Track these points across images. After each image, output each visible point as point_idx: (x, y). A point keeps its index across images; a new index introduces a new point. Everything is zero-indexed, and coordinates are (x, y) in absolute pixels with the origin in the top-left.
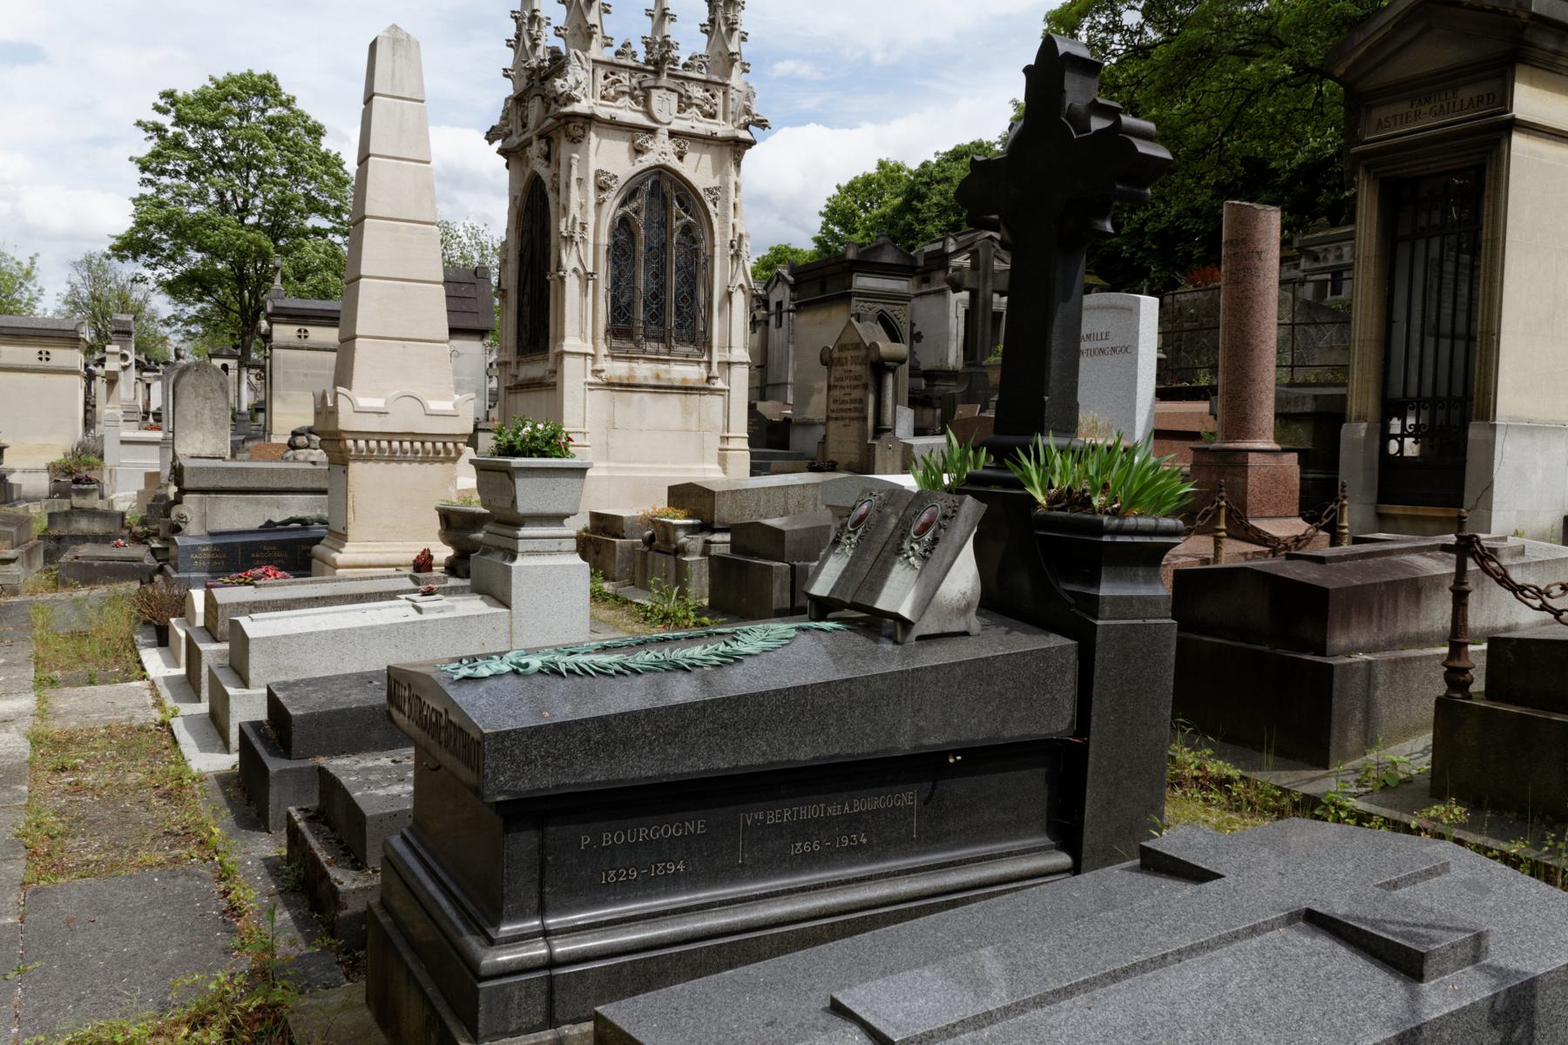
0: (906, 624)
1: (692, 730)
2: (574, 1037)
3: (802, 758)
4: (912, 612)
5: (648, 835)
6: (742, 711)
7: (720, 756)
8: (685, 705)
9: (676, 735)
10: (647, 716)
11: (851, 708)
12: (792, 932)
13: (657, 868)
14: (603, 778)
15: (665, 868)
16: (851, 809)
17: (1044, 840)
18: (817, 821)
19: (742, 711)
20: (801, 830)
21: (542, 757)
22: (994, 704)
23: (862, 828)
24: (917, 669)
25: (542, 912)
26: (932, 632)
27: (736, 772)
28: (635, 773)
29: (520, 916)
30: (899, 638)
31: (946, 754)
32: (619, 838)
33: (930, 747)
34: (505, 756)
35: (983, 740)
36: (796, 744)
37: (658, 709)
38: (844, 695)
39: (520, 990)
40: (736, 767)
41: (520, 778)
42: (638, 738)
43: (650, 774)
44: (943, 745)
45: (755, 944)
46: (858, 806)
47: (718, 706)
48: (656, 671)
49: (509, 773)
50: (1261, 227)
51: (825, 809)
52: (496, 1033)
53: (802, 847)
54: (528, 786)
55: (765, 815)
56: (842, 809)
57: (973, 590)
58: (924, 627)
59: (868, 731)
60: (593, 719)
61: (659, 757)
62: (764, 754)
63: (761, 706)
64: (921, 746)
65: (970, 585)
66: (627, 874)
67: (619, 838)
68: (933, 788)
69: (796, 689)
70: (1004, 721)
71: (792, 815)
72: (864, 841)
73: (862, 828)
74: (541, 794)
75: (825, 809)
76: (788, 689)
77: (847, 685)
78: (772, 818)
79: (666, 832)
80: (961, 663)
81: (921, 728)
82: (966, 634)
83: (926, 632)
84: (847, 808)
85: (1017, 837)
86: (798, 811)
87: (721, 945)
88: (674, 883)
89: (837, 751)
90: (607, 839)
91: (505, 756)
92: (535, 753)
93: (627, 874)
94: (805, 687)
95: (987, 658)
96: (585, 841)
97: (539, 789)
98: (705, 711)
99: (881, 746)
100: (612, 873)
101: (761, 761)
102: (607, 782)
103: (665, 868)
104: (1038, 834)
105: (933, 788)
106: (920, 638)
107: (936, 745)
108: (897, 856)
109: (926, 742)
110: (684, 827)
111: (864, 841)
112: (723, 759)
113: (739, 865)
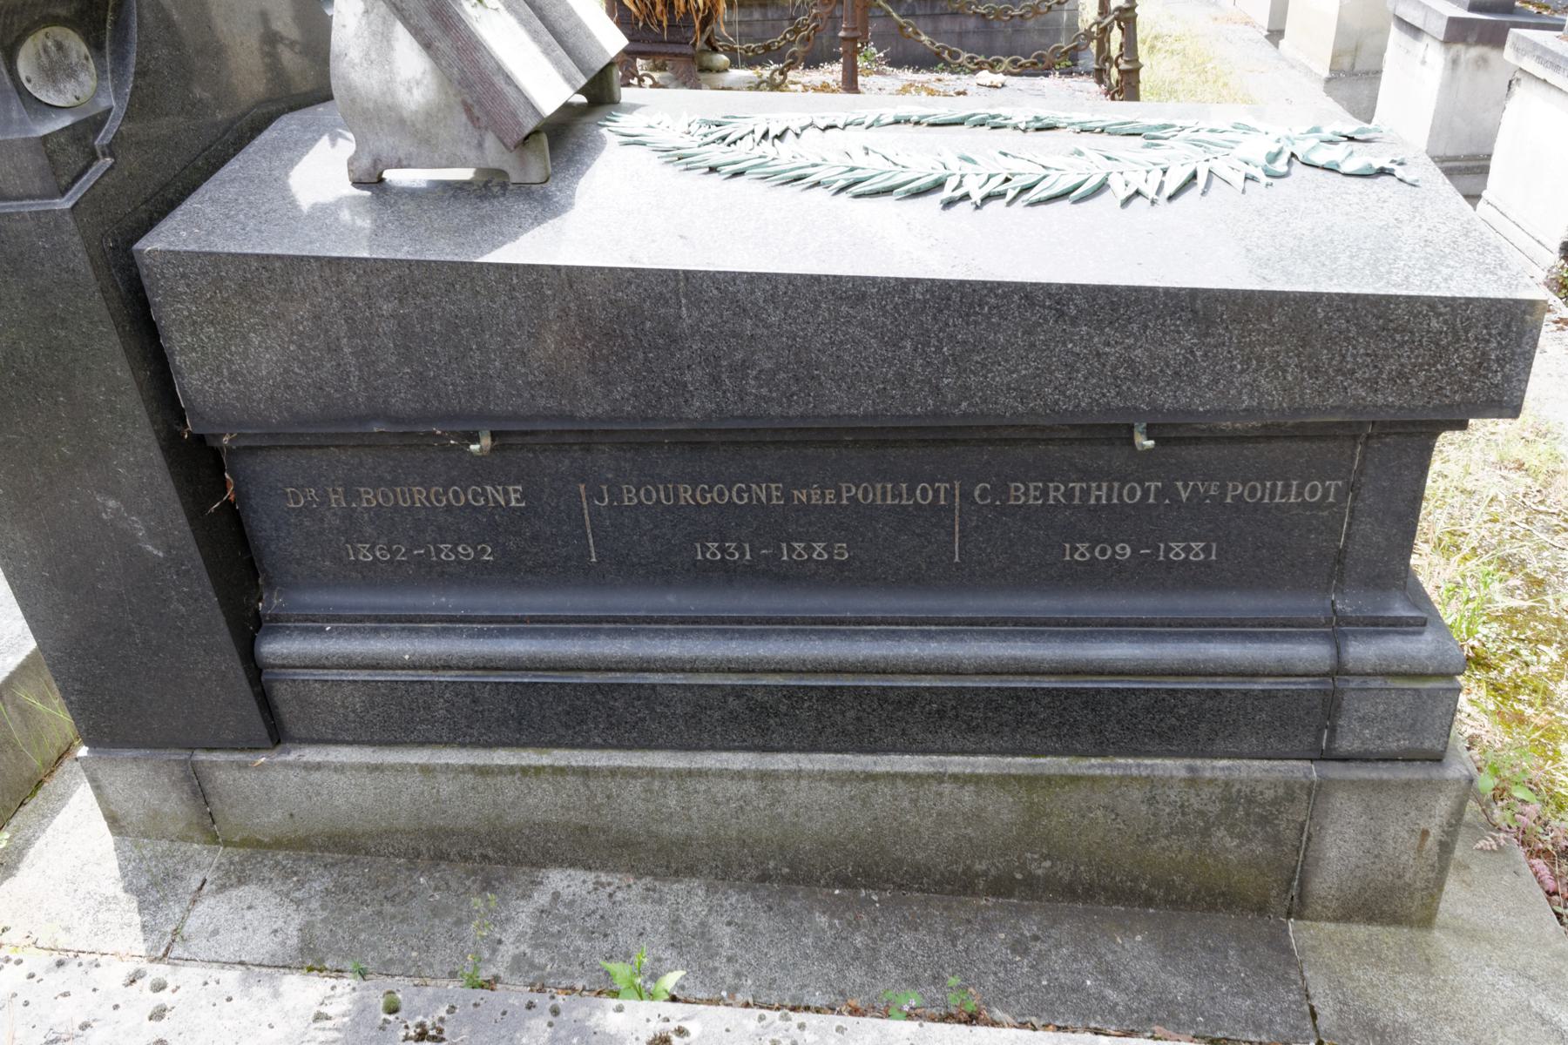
67: (648, 495)
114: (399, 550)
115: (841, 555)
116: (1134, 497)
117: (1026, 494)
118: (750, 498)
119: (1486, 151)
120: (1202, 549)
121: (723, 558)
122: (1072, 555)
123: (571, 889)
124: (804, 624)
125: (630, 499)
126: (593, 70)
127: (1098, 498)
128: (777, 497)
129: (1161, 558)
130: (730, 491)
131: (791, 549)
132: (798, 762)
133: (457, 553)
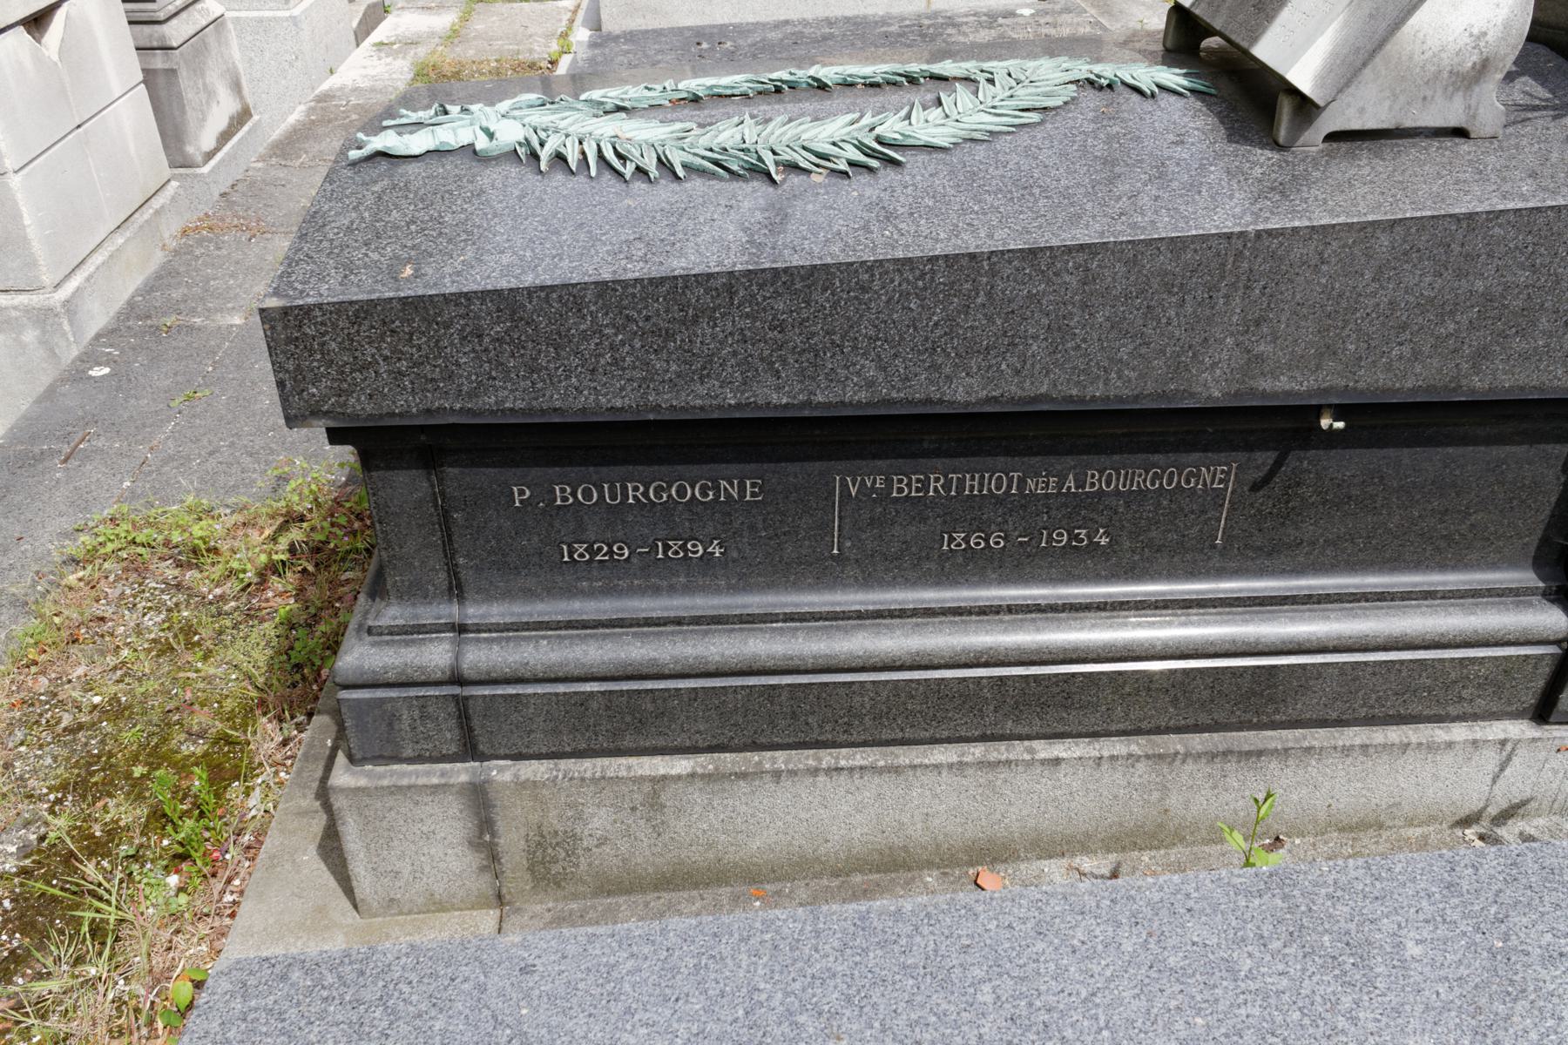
0: (1305, 107)
1: (704, 327)
2: (505, 785)
3: (961, 396)
4: (1321, 80)
5: (646, 494)
6: (820, 298)
7: (771, 381)
8: (686, 278)
9: (669, 336)
10: (600, 296)
11: (1084, 306)
12: (918, 681)
13: (667, 548)
14: (520, 405)
15: (683, 547)
16: (1080, 484)
17: (1526, 577)
18: (1000, 501)
19: (820, 298)
20: (971, 512)
21: (386, 359)
22: (1464, 319)
23: (1103, 519)
24: (1269, 232)
25: (456, 590)
26: (1371, 124)
27: (806, 413)
28: (586, 400)
29: (415, 592)
30: (1282, 134)
31: (1318, 411)
32: (587, 494)
33: (1275, 395)
34: (311, 352)
35: (1414, 390)
36: (947, 370)
37: (625, 284)
38: (1073, 281)
39: (410, 708)
40: (807, 404)
41: (349, 393)
42: (584, 336)
43: (619, 404)
44: (1309, 393)
45: (842, 691)
46: (1095, 481)
47: (761, 286)
48: (713, 175)
49: (324, 383)
50: (1273, 639)
51: (1022, 482)
52: (381, 757)
53: (967, 542)
54: (369, 408)
55: (889, 482)
56: (1060, 485)
57: (1507, 26)
58: (1351, 112)
59: (1123, 354)
60: (484, 295)
61: (638, 374)
62: (871, 384)
63: (864, 289)
64: (1252, 392)
65: (1502, 14)
66: (611, 552)
67: (587, 494)
68: (1278, 464)
69: (950, 260)
70: (1482, 354)
71: (948, 487)
72: (1104, 541)
73: (1103, 519)
74: (397, 422)
75: (1022, 482)
76: (933, 260)
77: (1080, 258)
78: (904, 486)
79: (681, 492)
80: (1394, 223)
81: (1260, 358)
82: (1460, 133)
83: (1356, 125)
84: (1071, 483)
85: (1459, 564)
86: (961, 482)
87: (773, 687)
88: (703, 573)
89: (1044, 389)
90: (561, 494)
91: (311, 352)
92: (370, 350)
93: (611, 552)
94: (972, 257)
95: (1471, 216)
96: (520, 495)
97: (392, 415)
98: (732, 294)
99: (1150, 387)
100: (581, 548)
101: (863, 396)
102: (529, 411)
103: (683, 547)
104: (1513, 564)
105: (1278, 464)
106: (1333, 137)
107: (1288, 394)
108: (1171, 575)
109: (1265, 384)
110: (717, 488)
111: (1104, 541)
112: (778, 388)
113: (833, 557)
114: (600, 549)
115: (997, 543)
116: (583, 490)
117: (909, 485)
118: (717, 496)
119: (1531, 46)
120: (586, 550)
121: (686, 555)
122: (949, 545)
123: (142, 899)
124: (528, 630)
125: (565, 499)
126: (1159, 32)
127: (973, 479)
128: (917, 488)
129: (660, 556)
130: (693, 488)
131: (667, 548)
132: (1504, 731)
133: (686, 551)
